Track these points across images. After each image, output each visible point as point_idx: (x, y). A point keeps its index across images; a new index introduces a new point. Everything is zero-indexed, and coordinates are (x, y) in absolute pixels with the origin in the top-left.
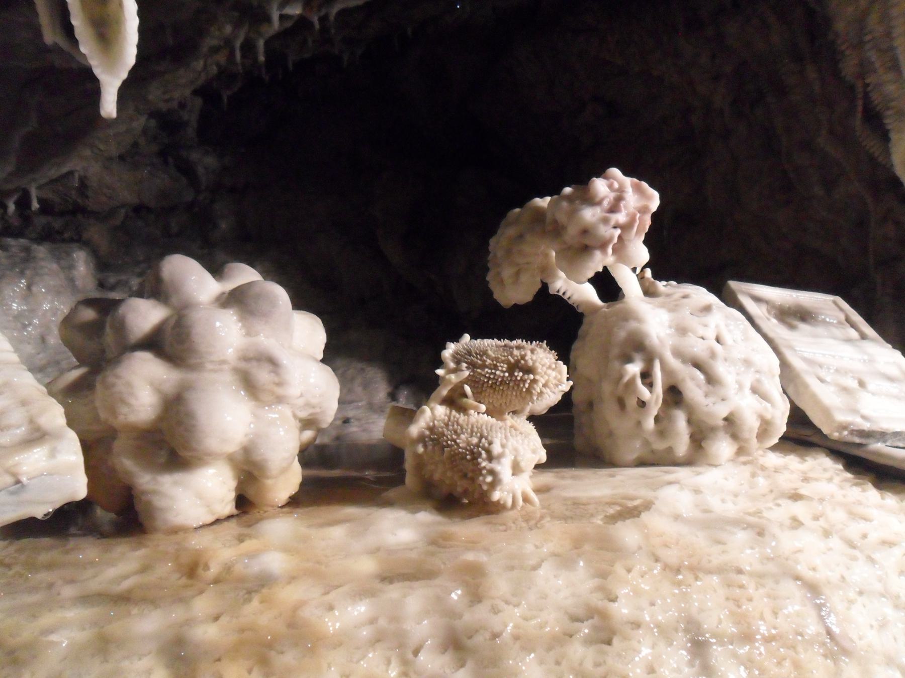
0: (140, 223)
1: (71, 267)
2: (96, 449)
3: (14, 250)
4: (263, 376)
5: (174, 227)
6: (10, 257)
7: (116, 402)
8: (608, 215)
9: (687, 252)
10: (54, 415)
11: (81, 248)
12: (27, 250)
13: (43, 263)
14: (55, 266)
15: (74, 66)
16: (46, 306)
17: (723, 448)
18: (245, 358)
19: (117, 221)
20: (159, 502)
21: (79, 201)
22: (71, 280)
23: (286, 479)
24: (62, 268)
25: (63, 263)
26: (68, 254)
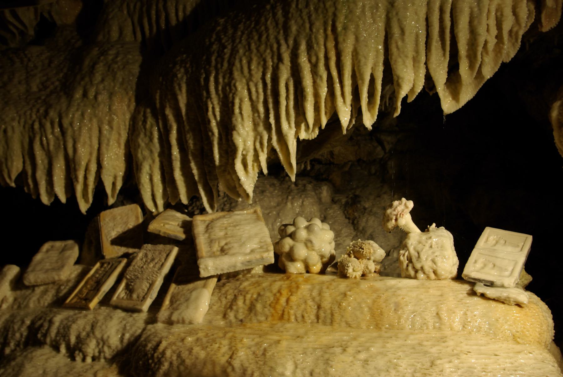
0: (359, 168)
1: (321, 193)
2: (277, 256)
3: (300, 186)
4: (309, 244)
5: (373, 171)
6: (298, 189)
7: (283, 247)
8: (310, 223)
9: (422, 220)
10: (272, 248)
11: (326, 184)
12: (304, 186)
13: (309, 192)
14: (313, 193)
15: (211, 138)
16: (308, 210)
17: (421, 275)
18: (306, 240)
19: (346, 169)
20: (288, 267)
21: (331, 160)
22: (320, 199)
23: (317, 267)
24: (316, 194)
25: (317, 192)
26: (320, 187)
